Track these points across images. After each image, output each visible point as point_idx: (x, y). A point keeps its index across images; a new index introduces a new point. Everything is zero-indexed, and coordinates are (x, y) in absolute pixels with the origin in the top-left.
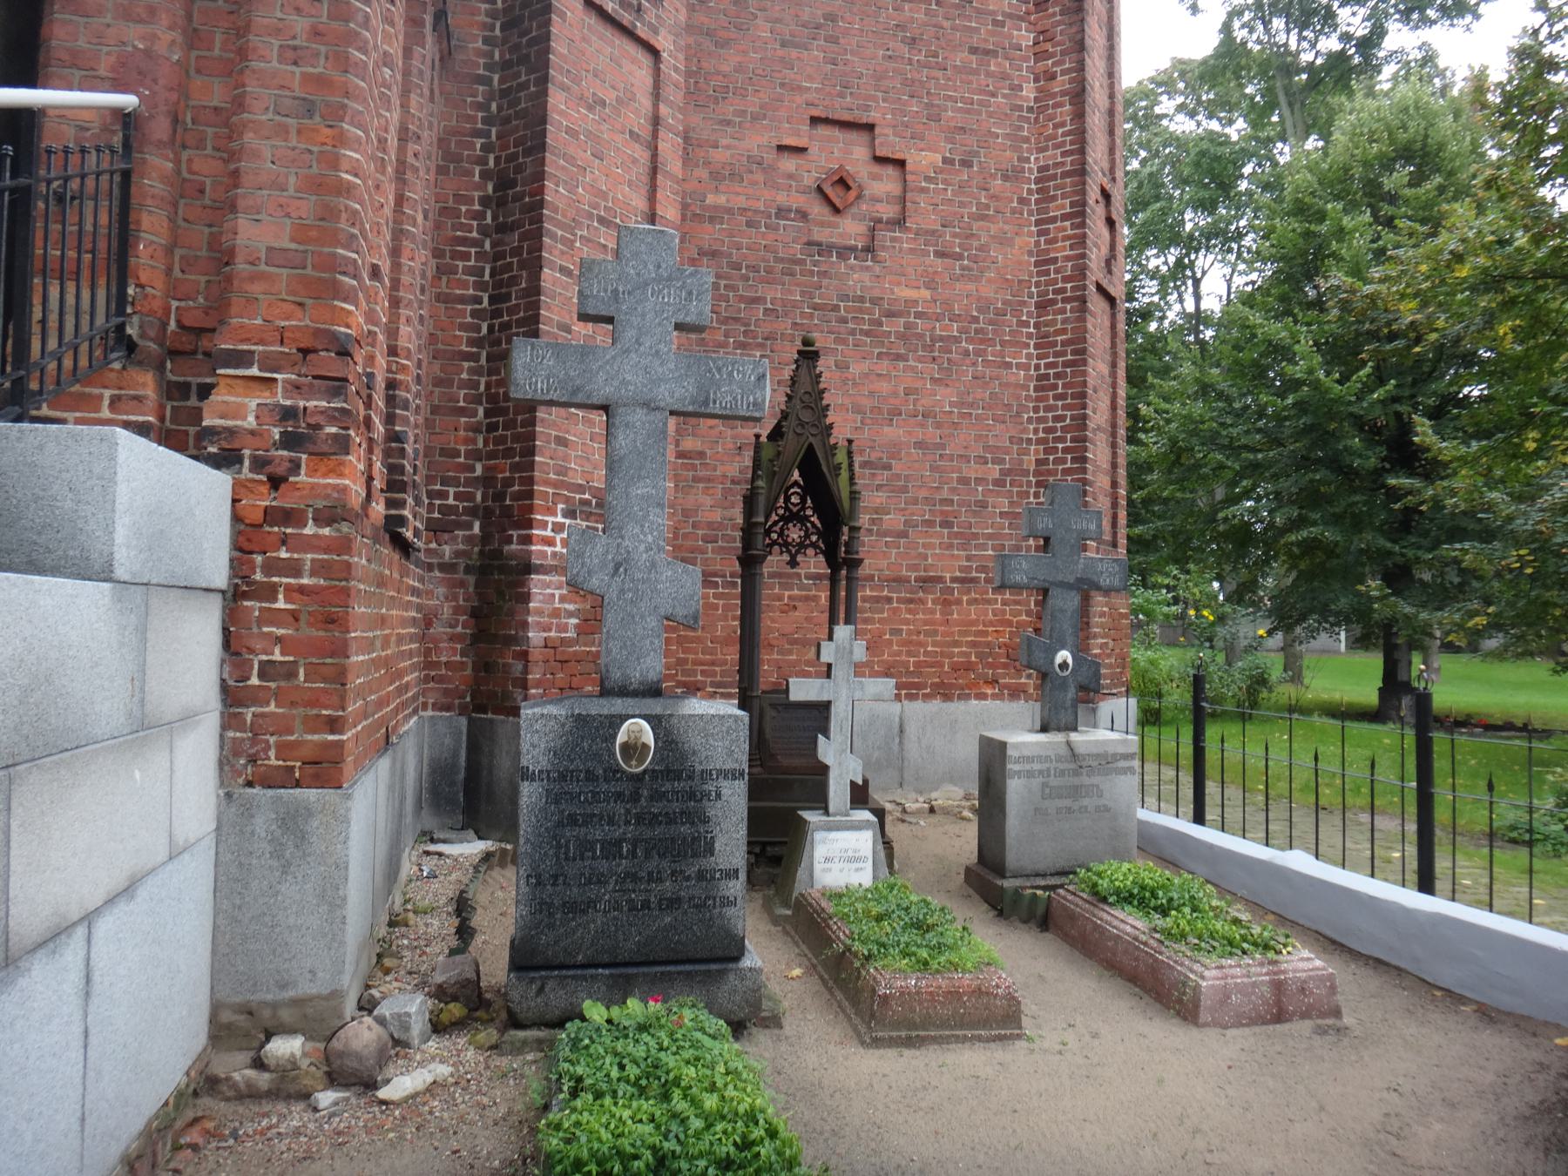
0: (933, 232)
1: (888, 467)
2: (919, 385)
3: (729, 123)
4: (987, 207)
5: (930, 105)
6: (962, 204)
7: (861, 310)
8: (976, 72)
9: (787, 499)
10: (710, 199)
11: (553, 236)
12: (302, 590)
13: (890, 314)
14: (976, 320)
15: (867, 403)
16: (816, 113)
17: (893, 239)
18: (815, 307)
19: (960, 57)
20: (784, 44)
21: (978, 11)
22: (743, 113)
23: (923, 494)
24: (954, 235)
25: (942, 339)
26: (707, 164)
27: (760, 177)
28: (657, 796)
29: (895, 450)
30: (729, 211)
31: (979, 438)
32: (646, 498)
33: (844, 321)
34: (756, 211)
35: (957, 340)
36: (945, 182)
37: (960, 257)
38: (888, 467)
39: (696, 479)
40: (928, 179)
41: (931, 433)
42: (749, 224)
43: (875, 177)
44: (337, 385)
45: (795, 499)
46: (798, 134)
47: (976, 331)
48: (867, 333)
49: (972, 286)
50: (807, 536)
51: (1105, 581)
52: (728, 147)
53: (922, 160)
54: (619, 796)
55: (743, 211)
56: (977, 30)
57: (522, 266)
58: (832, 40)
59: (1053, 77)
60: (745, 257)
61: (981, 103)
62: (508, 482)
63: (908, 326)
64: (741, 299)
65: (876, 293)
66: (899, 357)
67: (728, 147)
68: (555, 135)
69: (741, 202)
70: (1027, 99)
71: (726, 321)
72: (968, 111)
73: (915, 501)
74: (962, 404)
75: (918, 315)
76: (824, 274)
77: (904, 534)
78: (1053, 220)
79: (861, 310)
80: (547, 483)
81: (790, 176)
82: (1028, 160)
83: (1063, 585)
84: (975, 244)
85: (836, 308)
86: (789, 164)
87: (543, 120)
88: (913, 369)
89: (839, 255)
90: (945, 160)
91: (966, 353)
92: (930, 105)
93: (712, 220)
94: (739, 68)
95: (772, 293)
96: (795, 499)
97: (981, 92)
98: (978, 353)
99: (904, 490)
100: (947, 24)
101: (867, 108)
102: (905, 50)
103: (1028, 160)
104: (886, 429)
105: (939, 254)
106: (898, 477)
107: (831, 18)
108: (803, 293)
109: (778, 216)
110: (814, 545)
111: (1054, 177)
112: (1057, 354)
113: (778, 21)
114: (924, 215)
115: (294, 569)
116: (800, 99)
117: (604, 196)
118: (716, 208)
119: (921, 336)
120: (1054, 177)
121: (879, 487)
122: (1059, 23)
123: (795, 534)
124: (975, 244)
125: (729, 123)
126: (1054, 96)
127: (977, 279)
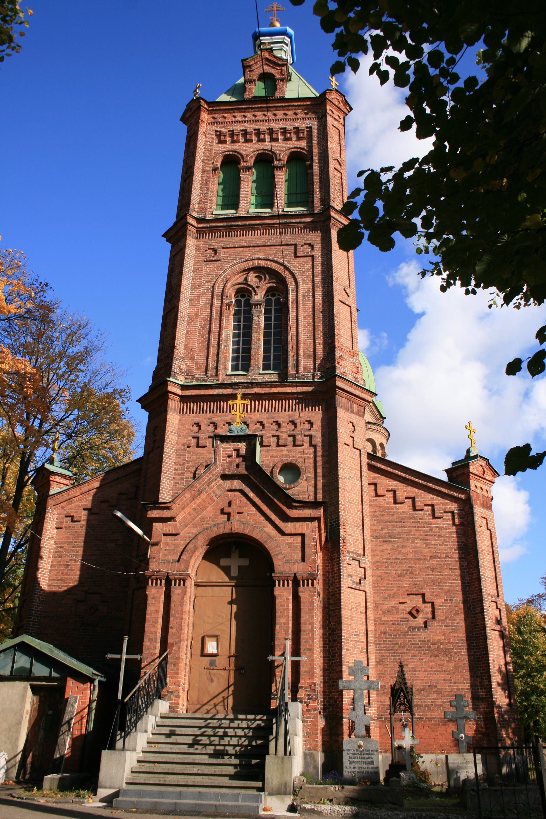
0: (443, 620)
1: (436, 687)
2: (442, 663)
3: (386, 598)
4: (458, 611)
5: (439, 586)
6: (451, 612)
7: (425, 644)
8: (452, 575)
9: (400, 699)
10: (383, 619)
11: (344, 643)
12: (312, 721)
13: (433, 644)
14: (457, 643)
15: (429, 669)
16: (409, 593)
17: (432, 624)
18: (412, 644)
19: (446, 572)
20: (399, 576)
21: (450, 558)
22: (389, 595)
23: (447, 693)
24: (450, 620)
25: (448, 649)
26: (381, 609)
27: (395, 611)
28: (364, 754)
29: (437, 682)
30: (388, 621)
31: (461, 676)
32: (361, 705)
33: (420, 647)
34: (395, 621)
35: (452, 649)
36: (445, 606)
37: (451, 626)
38: (436, 687)
39: (384, 693)
40: (441, 606)
41: (448, 677)
42: (393, 624)
43: (425, 607)
44: (314, 690)
45: (402, 699)
46: (404, 598)
47: (458, 646)
48: (427, 650)
49: (455, 634)
50: (406, 708)
51: (471, 717)
52: (386, 605)
53: (438, 601)
54: (358, 754)
55: (391, 621)
56: (450, 564)
57: (338, 649)
58: (411, 572)
59: (473, 574)
60: (393, 633)
61: (453, 583)
62: (337, 699)
63: (438, 647)
64: (393, 644)
65: (429, 639)
66: (436, 656)
67: (386, 605)
68: (344, 620)
69: (390, 618)
70: (467, 580)
71: (389, 650)
72: (450, 586)
73: (444, 696)
74: (456, 667)
75: (441, 643)
76: (414, 635)
77: (442, 705)
78: (477, 613)
79: (425, 644)
80: (346, 698)
81: (403, 610)
82: (469, 597)
83: (460, 718)
84: (455, 622)
85: (418, 644)
86: (402, 606)
87: (341, 617)
88: (441, 658)
89: (418, 629)
90: (445, 600)
91: (456, 653)
92: (439, 586)
93: (383, 624)
94: (388, 584)
95: (400, 642)
96: (402, 699)
97: (454, 580)
98: (459, 652)
99: (441, 693)
100: (442, 563)
101: (422, 589)
102: (431, 572)
103: (469, 597)
104: (435, 676)
105: (445, 626)
106: (439, 689)
107: (411, 567)
108: (409, 641)
109: (401, 621)
110: (407, 710)
111: (476, 602)
112: (481, 651)
113: (397, 570)
114: (440, 615)
115: (310, 718)
116: (404, 590)
117: (355, 629)
118: (384, 621)
119: (442, 649)
120: (476, 602)
121: (434, 692)
122: (473, 559)
123: (402, 707)
124: (455, 622)
125: (386, 598)
126: (473, 579)
127: (457, 632)
